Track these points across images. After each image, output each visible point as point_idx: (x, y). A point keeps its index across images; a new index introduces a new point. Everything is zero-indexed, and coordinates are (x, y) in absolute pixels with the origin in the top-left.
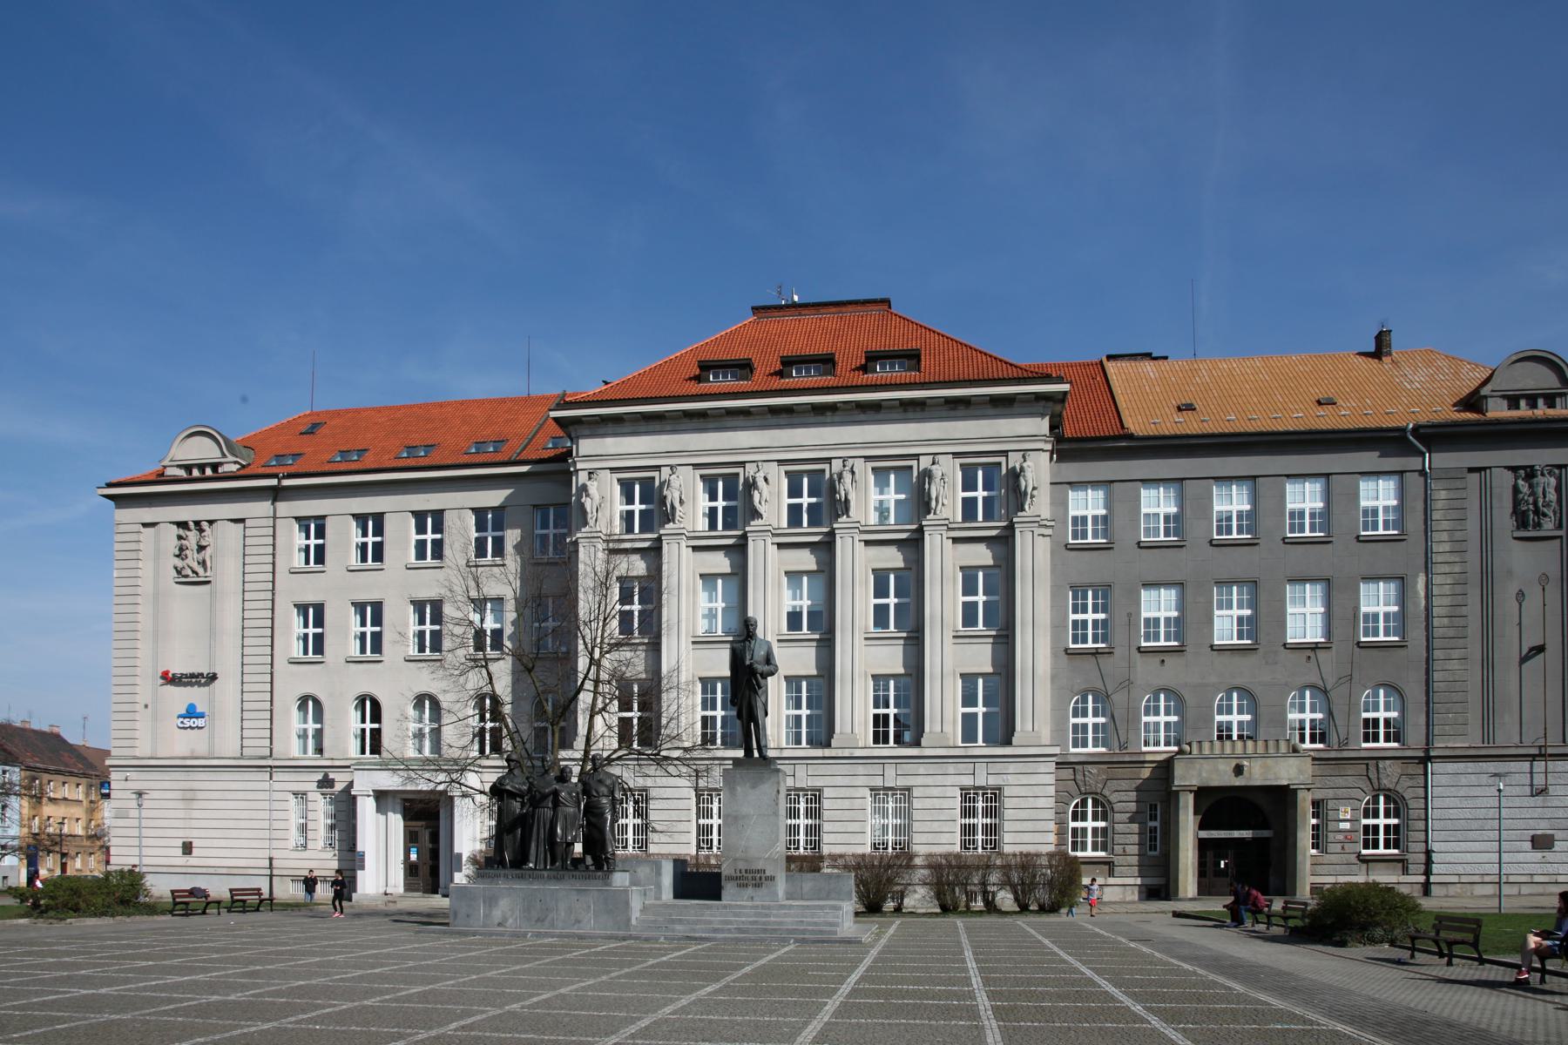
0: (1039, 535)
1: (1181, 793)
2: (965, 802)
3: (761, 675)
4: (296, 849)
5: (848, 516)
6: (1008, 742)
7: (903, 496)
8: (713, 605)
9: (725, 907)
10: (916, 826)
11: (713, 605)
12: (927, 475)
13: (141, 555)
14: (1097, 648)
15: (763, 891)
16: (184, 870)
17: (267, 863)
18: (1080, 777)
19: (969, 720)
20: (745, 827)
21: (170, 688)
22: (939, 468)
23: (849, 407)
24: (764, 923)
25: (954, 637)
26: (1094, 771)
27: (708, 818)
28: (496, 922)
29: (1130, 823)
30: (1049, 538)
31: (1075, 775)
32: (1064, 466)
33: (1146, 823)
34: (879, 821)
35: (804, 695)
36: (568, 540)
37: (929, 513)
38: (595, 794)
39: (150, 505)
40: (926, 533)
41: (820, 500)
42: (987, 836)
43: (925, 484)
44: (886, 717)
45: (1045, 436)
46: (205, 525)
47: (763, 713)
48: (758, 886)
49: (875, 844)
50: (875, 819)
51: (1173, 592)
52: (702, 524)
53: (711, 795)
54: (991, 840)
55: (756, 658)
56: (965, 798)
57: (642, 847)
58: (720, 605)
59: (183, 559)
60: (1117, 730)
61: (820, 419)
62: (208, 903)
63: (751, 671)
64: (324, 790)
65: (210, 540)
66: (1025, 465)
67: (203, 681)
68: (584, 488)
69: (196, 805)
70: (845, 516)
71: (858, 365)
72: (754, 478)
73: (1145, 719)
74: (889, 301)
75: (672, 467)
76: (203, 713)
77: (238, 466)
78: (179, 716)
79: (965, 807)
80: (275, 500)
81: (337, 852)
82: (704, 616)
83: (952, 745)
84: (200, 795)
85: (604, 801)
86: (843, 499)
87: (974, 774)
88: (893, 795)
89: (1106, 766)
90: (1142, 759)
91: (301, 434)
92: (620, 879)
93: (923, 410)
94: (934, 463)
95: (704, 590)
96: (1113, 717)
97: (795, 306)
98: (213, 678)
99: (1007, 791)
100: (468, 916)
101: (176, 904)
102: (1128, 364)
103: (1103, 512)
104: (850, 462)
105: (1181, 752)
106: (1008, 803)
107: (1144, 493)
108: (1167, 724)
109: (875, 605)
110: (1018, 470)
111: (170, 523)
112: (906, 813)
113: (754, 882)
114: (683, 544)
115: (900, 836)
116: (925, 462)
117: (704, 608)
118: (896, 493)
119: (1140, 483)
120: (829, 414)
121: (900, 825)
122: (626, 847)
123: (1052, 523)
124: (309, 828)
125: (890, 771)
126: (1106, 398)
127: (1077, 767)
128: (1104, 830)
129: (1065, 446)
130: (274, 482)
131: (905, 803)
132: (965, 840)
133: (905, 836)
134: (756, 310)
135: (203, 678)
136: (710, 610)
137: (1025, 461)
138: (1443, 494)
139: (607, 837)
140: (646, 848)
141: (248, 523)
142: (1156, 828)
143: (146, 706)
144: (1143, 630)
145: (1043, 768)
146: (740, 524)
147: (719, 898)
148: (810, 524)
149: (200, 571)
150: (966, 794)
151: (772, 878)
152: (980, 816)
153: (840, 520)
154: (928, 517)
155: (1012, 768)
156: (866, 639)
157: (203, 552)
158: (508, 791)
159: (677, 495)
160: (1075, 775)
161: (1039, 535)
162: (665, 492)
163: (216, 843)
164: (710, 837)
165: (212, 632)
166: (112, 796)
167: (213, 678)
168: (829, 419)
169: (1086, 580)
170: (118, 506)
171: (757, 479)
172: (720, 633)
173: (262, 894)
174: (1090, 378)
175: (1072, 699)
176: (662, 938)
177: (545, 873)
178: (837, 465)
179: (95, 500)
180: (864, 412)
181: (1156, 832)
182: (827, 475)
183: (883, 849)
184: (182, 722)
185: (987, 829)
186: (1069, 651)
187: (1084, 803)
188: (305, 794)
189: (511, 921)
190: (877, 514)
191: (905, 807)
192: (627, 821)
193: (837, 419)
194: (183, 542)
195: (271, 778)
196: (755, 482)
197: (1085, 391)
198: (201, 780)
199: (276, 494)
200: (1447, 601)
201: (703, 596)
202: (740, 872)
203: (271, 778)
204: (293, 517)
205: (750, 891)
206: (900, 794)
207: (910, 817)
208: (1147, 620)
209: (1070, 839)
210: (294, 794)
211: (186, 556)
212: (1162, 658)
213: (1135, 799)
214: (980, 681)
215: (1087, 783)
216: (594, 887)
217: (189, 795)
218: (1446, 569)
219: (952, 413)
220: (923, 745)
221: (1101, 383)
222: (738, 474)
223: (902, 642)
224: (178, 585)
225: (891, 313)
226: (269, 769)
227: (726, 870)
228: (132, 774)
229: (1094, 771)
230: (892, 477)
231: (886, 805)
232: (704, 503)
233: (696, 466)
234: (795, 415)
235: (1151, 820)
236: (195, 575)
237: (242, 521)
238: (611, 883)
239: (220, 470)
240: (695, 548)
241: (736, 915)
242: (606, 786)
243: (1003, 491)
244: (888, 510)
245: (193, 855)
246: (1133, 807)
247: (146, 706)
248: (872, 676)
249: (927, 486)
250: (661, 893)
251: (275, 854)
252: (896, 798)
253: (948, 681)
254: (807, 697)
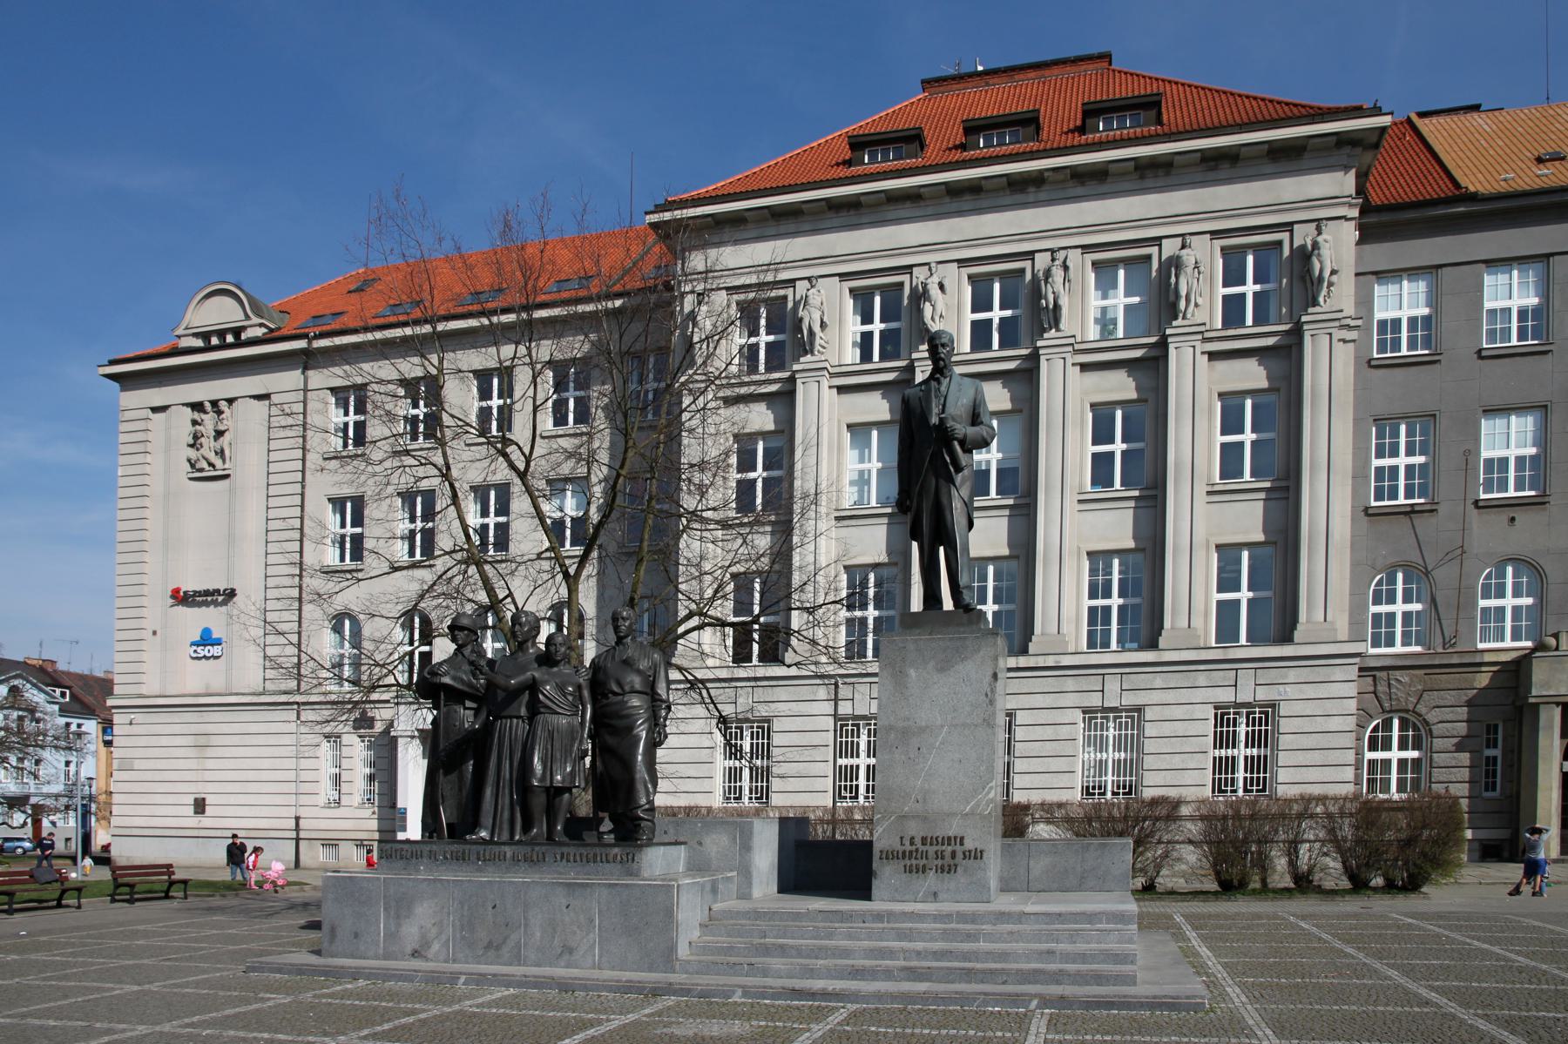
0: (1339, 340)
1: (1542, 706)
2: (1222, 726)
3: (962, 443)
4: (328, 805)
5: (1058, 330)
6: (1286, 637)
7: (1136, 300)
8: (865, 466)
9: (879, 917)
10: (1149, 762)
11: (865, 466)
12: (1175, 263)
13: (149, 447)
14: (1412, 505)
15: (960, 878)
16: (195, 833)
17: (292, 824)
18: (1382, 688)
19: (1227, 611)
20: (924, 750)
21: (181, 609)
22: (1192, 253)
23: (1060, 176)
24: (966, 956)
25: (1209, 493)
26: (1405, 679)
27: (846, 757)
28: (409, 950)
29: (1457, 751)
30: (1352, 344)
31: (1375, 685)
32: (1371, 249)
33: (1480, 752)
34: (1092, 755)
35: (990, 584)
36: (758, 580)
37: (1176, 318)
38: (615, 688)
39: (160, 384)
40: (1170, 345)
41: (1018, 312)
42: (1252, 772)
43: (1170, 278)
44: (1107, 610)
45: (1350, 196)
46: (223, 405)
47: (964, 522)
48: (949, 869)
49: (1088, 787)
50: (1089, 753)
51: (1530, 420)
52: (851, 356)
53: (858, 726)
54: (1258, 778)
55: (950, 409)
56: (1220, 719)
57: (761, 798)
58: (875, 465)
59: (198, 450)
60: (1439, 620)
61: (1020, 198)
62: (64, 892)
63: (943, 435)
64: (362, 731)
65: (229, 423)
66: (1320, 239)
67: (220, 599)
68: (692, 316)
69: (210, 752)
70: (1054, 330)
71: (1072, 126)
72: (925, 285)
73: (1483, 603)
74: (1111, 55)
75: (809, 279)
76: (220, 639)
77: (265, 330)
78: (193, 644)
79: (1222, 732)
80: (305, 368)
81: (376, 809)
82: (852, 483)
83: (1202, 646)
84: (215, 740)
85: (635, 701)
86: (1051, 306)
87: (1236, 686)
88: (1115, 718)
89: (1422, 672)
90: (1478, 660)
91: (350, 292)
92: (658, 861)
93: (1168, 174)
94: (1183, 247)
95: (853, 446)
96: (1433, 601)
97: (980, 74)
98: (231, 594)
99: (1284, 709)
100: (356, 935)
101: (118, 886)
102: (1448, 120)
103: (1425, 311)
104: (1061, 255)
105: (1540, 647)
106: (1285, 725)
107: (1488, 280)
108: (1516, 609)
109: (1093, 454)
110: (1310, 247)
111: (183, 405)
112: (1134, 744)
113: (939, 862)
114: (825, 383)
115: (1125, 776)
116: (1170, 248)
117: (851, 470)
118: (1127, 295)
119: (1483, 266)
120: (1032, 189)
121: (1125, 760)
122: (740, 798)
123: (1359, 322)
124: (342, 779)
125: (1113, 685)
126: (1424, 159)
127: (1378, 674)
128: (1417, 762)
129: (1372, 219)
130: (302, 344)
131: (1132, 729)
132: (1220, 779)
133: (1131, 776)
134: (927, 84)
135: (220, 595)
136: (861, 473)
137: (1320, 233)
139: (638, 776)
140: (767, 798)
141: (275, 399)
142: (1495, 758)
143: (155, 633)
144: (1482, 477)
145: (1338, 674)
146: (904, 352)
147: (866, 895)
148: (1002, 346)
149: (218, 462)
150: (1223, 715)
151: (978, 855)
152: (1242, 745)
153: (1046, 336)
154: (1175, 323)
155: (1292, 675)
156: (1080, 501)
157: (221, 439)
158: (446, 686)
159: (816, 316)
160: (1375, 685)
161: (1339, 340)
162: (801, 313)
163: (232, 799)
164: (854, 783)
165: (231, 539)
166: (114, 744)
167: (231, 594)
168: (1031, 198)
169: (1398, 409)
170: (123, 389)
171: (929, 287)
172: (873, 503)
173: (173, 873)
174: (1396, 140)
176: (739, 992)
177: (509, 851)
178: (1042, 261)
179: (90, 375)
180: (1083, 184)
181: (1495, 764)
182: (1028, 276)
183: (1099, 794)
184: (195, 651)
185: (1250, 763)
186: (1370, 511)
187: (1387, 725)
188: (339, 737)
189: (436, 947)
190: (1098, 328)
191: (1132, 735)
193: (1043, 196)
194: (198, 427)
195: (298, 718)
196: (926, 292)
197: (1392, 154)
198: (217, 722)
199: (307, 360)
201: (851, 456)
202: (912, 843)
203: (298, 718)
204: (328, 389)
205: (931, 880)
206: (1126, 717)
207: (1140, 750)
208: (1489, 462)
209: (1365, 777)
210: (326, 737)
211: (201, 445)
212: (1511, 515)
213: (1465, 717)
214: (1245, 555)
215: (1394, 697)
216: (602, 879)
217: (202, 740)
219: (1211, 175)
220: (1160, 646)
221: (1413, 143)
222: (901, 284)
223: (1132, 504)
224: (192, 482)
225: (1114, 71)
226: (296, 707)
227: (883, 838)
228: (138, 717)
229: (1405, 679)
230: (1121, 273)
231: (1105, 733)
232: (854, 327)
233: (843, 276)
234: (983, 195)
235: (1488, 747)
236: (211, 468)
237: (266, 397)
238: (639, 869)
239: (243, 336)
240: (842, 389)
241: (902, 935)
242: (639, 672)
243: (1285, 281)
244: (1114, 322)
245: (207, 814)
246: (1462, 728)
247: (155, 633)
248: (1089, 554)
249: (1173, 279)
250: (750, 884)
251: (303, 812)
252: (1121, 723)
253: (1199, 555)
254: (995, 588)
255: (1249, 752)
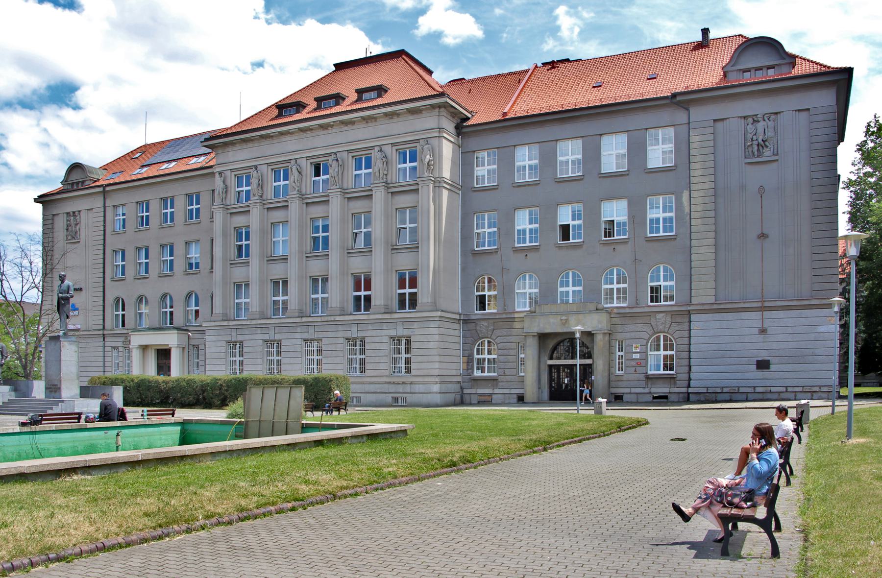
6: (414, 308)
73: (625, 286)
93: (376, 121)
120: (330, 128)
124: (366, 362)
138: (697, 138)
141: (812, 112)
175: (673, 268)
192: (356, 356)
200: (700, 208)
218: (700, 187)
229: (486, 324)
234: (314, 131)
237: (808, 110)
255: (312, 357)
